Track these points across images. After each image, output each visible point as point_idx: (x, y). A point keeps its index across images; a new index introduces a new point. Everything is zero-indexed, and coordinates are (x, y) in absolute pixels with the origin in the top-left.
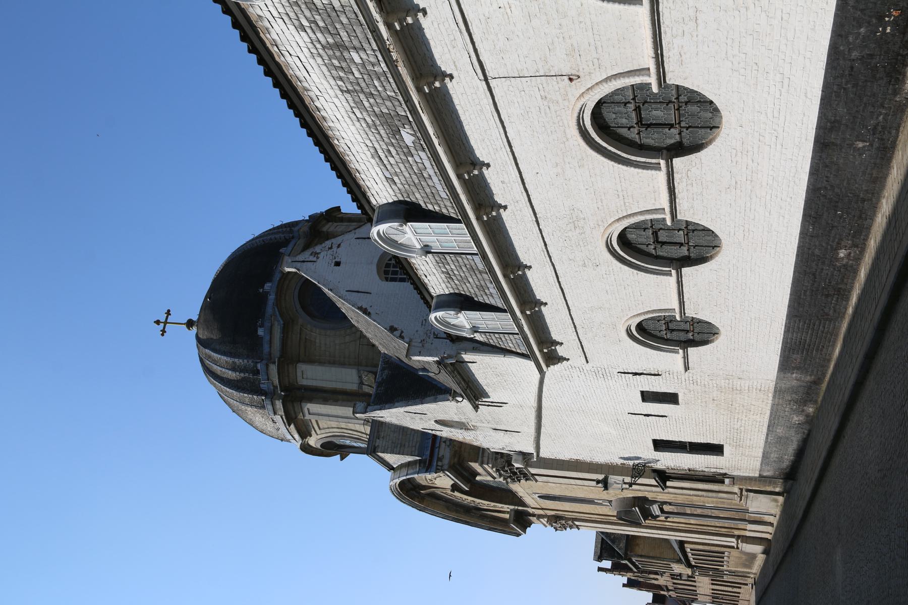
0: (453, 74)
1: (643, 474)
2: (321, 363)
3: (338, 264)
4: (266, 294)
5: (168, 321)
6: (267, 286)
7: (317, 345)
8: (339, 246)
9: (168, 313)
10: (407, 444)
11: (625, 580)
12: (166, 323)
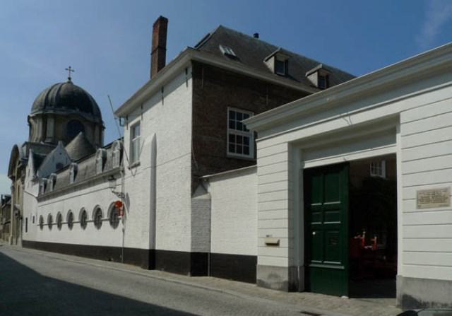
0: (223, 25)
4: (75, 109)
6: (78, 110)
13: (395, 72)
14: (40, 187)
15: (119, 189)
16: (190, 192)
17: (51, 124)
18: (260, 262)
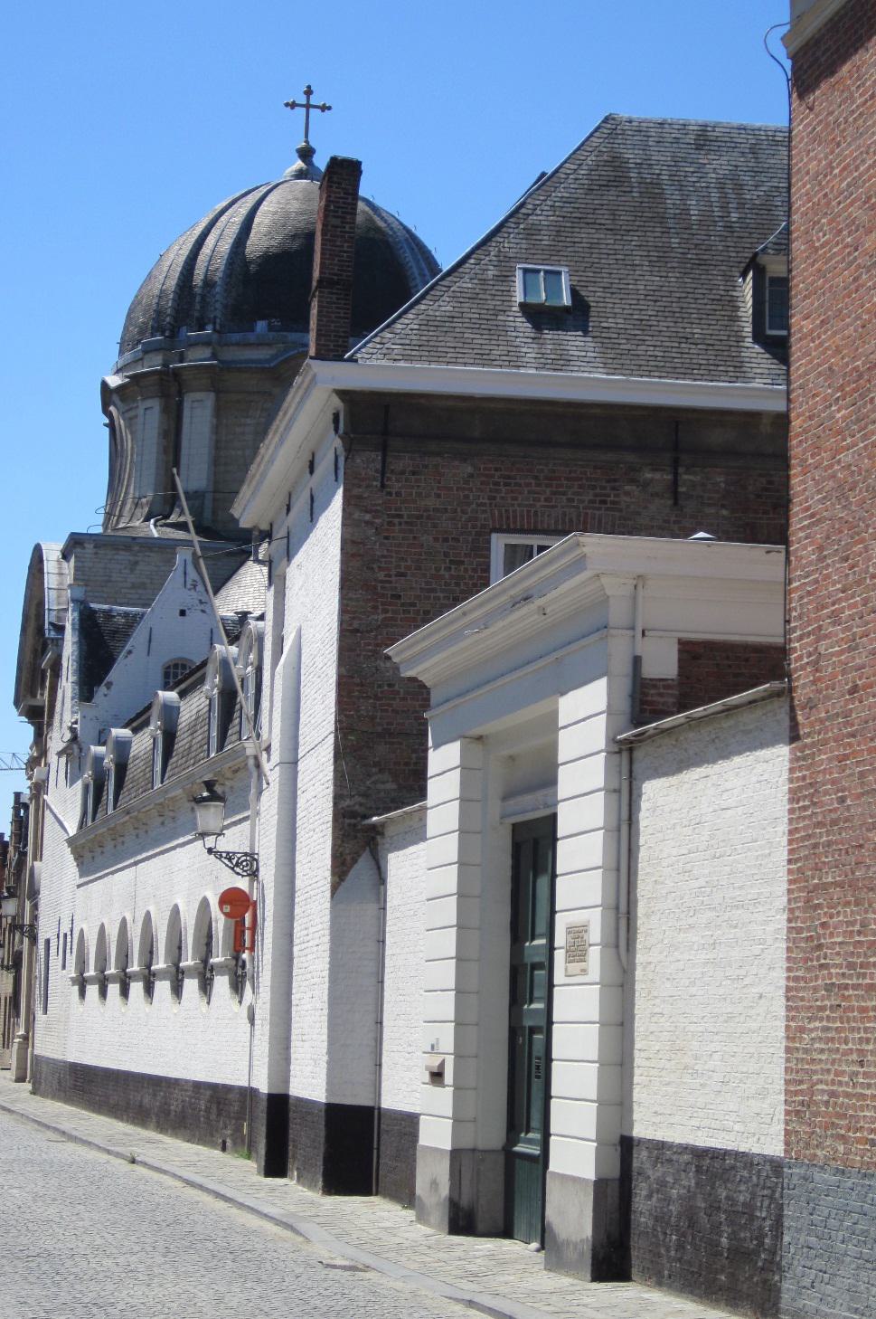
1: (238, 874)
2: (216, 429)
3: (183, 613)
7: (243, 420)
8: (203, 611)
10: (89, 588)
12: (308, 106)
13: (519, 634)
14: (86, 788)
17: (199, 414)
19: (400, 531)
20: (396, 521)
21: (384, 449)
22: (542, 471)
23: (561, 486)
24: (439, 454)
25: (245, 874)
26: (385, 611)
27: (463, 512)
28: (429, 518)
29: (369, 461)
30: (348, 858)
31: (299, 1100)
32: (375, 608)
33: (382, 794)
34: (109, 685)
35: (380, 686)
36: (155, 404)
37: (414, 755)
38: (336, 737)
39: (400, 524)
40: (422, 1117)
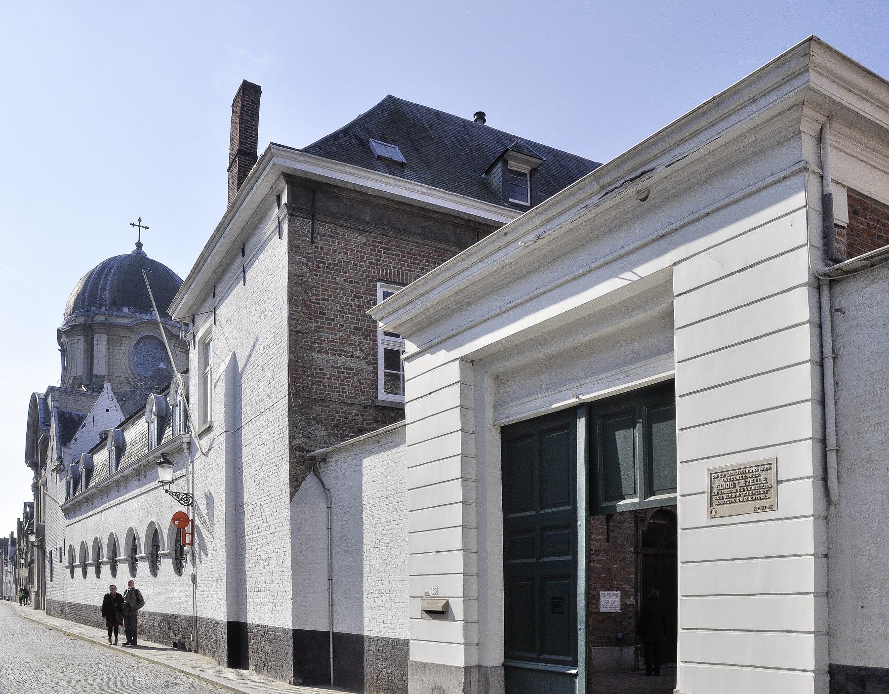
1: (182, 504)
3: (107, 411)
5: (141, 228)
7: (119, 348)
9: (146, 228)
11: (21, 520)
12: (140, 226)
14: (68, 483)
15: (180, 487)
16: (287, 489)
18: (416, 655)
19: (324, 272)
20: (321, 265)
21: (313, 218)
22: (405, 248)
23: (416, 259)
24: (346, 227)
25: (186, 504)
26: (317, 322)
27: (361, 266)
28: (340, 266)
29: (305, 225)
30: (300, 477)
31: (256, 626)
32: (310, 318)
33: (318, 438)
34: (76, 440)
35: (315, 369)
36: (82, 338)
37: (337, 415)
38: (289, 399)
39: (324, 267)
40: (411, 641)
